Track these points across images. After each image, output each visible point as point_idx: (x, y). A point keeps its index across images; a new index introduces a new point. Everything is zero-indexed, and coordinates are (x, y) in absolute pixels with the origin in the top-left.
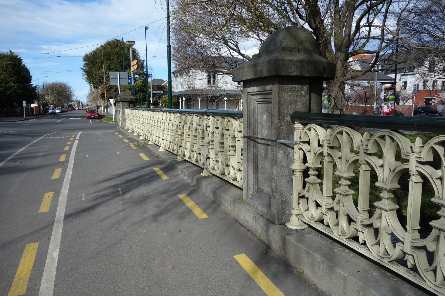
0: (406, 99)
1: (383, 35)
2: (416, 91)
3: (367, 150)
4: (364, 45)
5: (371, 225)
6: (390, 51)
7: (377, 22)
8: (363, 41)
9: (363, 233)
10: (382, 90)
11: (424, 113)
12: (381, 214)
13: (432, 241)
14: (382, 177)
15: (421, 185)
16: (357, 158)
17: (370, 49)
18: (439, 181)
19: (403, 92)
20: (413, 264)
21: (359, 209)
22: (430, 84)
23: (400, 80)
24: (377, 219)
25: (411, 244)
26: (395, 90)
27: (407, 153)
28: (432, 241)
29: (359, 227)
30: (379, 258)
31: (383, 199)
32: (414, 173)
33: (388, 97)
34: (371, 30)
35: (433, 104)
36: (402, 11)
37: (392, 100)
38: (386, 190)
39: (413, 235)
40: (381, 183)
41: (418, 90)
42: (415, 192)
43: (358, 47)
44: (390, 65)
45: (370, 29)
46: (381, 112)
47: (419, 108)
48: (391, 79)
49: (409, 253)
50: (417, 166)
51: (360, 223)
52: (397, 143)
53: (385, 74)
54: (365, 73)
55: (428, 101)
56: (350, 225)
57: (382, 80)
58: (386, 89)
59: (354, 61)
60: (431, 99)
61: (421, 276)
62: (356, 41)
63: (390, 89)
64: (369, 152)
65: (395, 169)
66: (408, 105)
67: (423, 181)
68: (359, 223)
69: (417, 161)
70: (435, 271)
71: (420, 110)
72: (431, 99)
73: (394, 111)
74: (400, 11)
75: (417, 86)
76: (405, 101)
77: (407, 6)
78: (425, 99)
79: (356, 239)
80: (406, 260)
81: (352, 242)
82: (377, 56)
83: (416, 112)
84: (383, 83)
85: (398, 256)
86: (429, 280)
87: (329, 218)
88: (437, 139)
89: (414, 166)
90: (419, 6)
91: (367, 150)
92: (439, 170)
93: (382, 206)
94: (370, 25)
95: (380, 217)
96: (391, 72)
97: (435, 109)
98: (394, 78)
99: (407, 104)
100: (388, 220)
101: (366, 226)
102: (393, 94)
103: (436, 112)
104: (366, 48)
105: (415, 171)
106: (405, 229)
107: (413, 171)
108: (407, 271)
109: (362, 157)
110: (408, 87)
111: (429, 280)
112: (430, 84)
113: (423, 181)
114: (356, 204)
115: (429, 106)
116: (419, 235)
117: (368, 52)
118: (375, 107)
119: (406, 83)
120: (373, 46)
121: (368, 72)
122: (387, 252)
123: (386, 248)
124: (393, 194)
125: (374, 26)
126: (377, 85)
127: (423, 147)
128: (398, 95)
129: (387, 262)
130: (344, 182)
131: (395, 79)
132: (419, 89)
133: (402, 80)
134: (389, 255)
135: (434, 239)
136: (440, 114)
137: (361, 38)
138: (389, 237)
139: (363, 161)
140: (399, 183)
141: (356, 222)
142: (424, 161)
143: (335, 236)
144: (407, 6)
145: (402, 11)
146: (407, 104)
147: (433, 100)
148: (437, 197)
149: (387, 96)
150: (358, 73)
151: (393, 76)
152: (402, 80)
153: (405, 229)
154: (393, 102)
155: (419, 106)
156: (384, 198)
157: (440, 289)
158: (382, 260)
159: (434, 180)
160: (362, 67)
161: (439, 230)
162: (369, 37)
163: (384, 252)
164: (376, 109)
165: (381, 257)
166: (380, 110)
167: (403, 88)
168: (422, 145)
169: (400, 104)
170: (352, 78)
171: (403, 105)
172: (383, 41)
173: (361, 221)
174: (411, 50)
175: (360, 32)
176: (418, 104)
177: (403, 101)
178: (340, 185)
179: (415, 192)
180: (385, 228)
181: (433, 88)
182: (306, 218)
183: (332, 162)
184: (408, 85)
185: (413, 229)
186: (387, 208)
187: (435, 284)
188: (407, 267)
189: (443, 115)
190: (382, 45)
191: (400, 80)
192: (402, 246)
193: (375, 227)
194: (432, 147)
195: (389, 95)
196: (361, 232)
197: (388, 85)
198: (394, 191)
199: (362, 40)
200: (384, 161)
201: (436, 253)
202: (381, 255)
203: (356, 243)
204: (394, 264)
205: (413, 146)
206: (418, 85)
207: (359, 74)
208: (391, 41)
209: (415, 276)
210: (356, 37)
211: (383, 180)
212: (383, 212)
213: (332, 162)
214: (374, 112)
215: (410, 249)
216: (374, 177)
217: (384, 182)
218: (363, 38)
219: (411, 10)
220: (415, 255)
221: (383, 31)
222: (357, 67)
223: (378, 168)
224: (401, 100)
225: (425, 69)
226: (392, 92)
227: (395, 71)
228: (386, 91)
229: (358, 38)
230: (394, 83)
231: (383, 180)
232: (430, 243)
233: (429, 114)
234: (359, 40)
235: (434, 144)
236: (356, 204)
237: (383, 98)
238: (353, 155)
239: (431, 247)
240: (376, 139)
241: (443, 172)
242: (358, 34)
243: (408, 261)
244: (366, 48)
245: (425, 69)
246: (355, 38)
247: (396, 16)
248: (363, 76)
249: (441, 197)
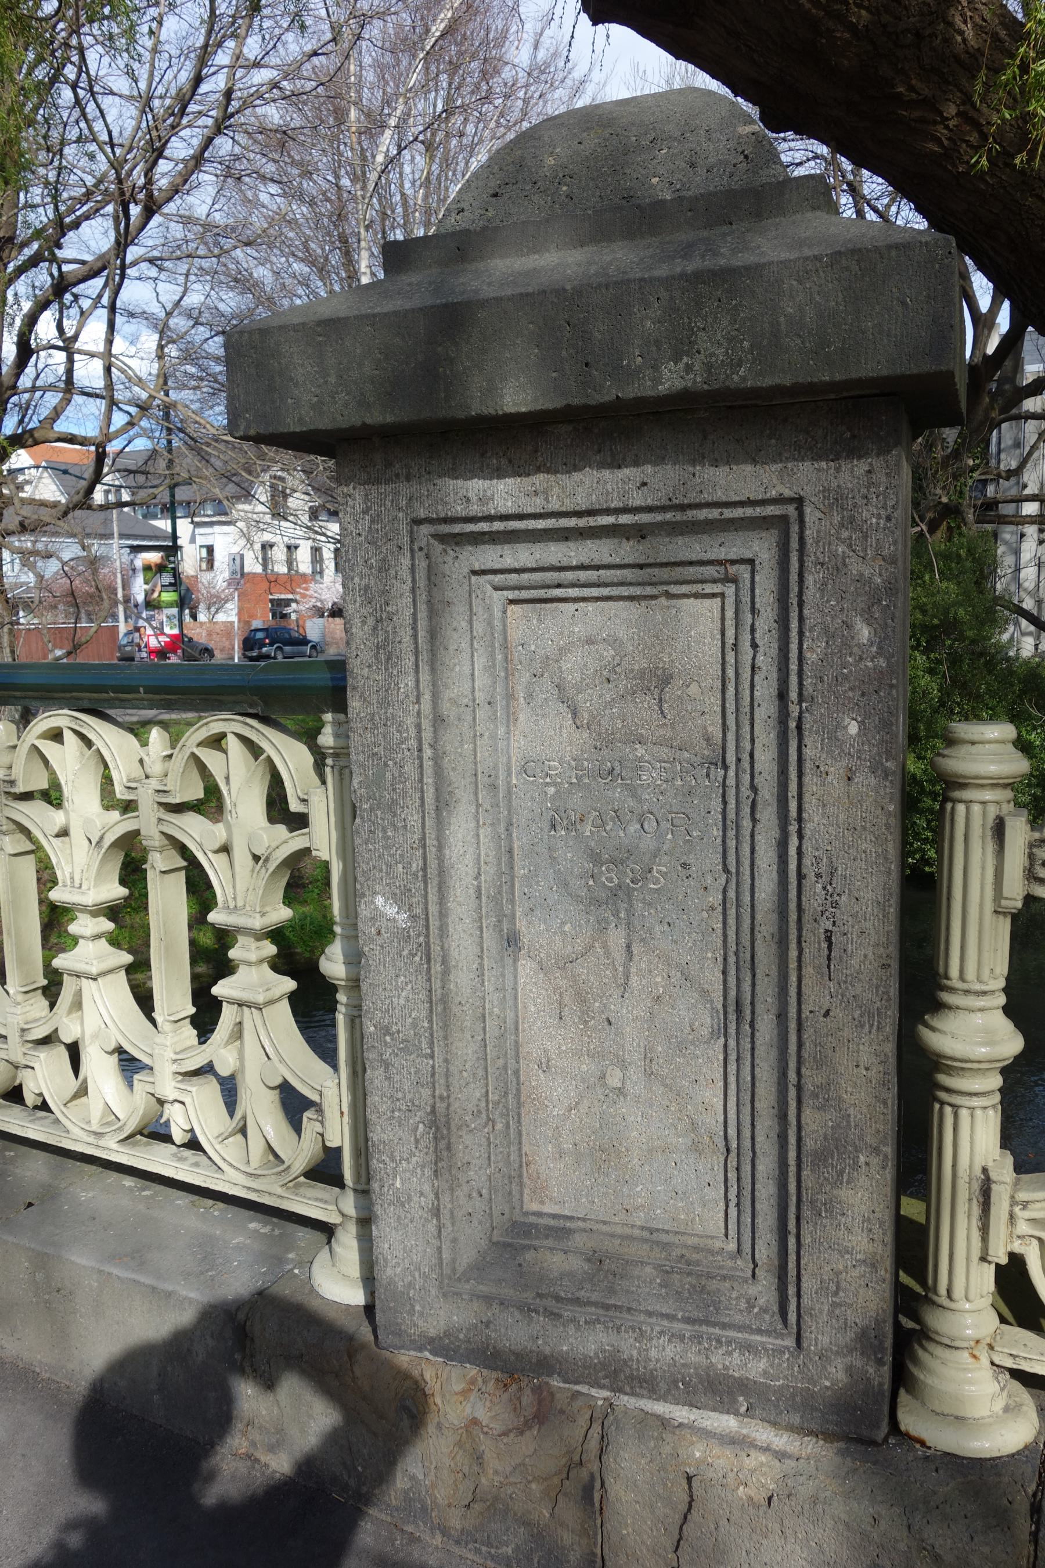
0: (217, 602)
1: (110, 386)
2: (239, 576)
3: (12, 783)
4: (57, 413)
5: (208, 1069)
6: (141, 444)
7: (93, 334)
8: (52, 399)
9: (183, 1103)
10: (134, 570)
11: (271, 644)
12: (79, 993)
13: (227, 1044)
14: (68, 870)
15: (182, 874)
16: (128, 825)
17: (74, 430)
18: (223, 856)
19: (205, 578)
20: (188, 1128)
21: (11, 992)
22: (279, 554)
23: (193, 540)
24: (70, 1012)
25: (175, 1068)
26: (175, 573)
27: (129, 781)
28: (227, 1044)
29: (168, 1088)
30: (91, 1139)
31: (81, 941)
32: (157, 844)
33: (156, 595)
34: (76, 365)
35: (293, 616)
36: (169, 314)
37: (170, 605)
38: (84, 909)
39: (176, 1039)
40: (69, 889)
41: (243, 574)
42: (168, 902)
43: (35, 418)
44: (152, 490)
45: (70, 361)
46: (139, 646)
47: (257, 630)
48: (157, 535)
49: (171, 1099)
50: (160, 820)
51: (18, 1039)
52: (98, 750)
53: (145, 516)
54: (65, 514)
55: (279, 608)
56: (131, 1085)
57: (136, 537)
58: (147, 568)
59: (37, 467)
60: (287, 603)
61: (210, 1158)
62: (26, 396)
63: (161, 568)
64: (20, 788)
65: (102, 838)
66: (223, 623)
67: (185, 864)
68: (14, 1038)
69: (160, 804)
70: (243, 1131)
71: (260, 635)
72: (287, 603)
73: (179, 642)
74: (163, 315)
75: (238, 562)
76: (213, 609)
77: (181, 299)
78: (272, 601)
79: (157, 1133)
80: (168, 1121)
81: (9, 1112)
82: (100, 457)
83: (249, 643)
84: (136, 549)
85: (144, 1116)
86: (231, 1165)
87: (196, 1111)
88: (204, 729)
89: (154, 820)
90: (222, 306)
91: (12, 783)
92: (220, 825)
93: (80, 967)
94: (68, 345)
95: (77, 1004)
96: (162, 512)
97: (301, 631)
98: (170, 530)
99: (221, 617)
100: (102, 1010)
101: (197, 1073)
102: (171, 584)
103: (304, 641)
104: (62, 426)
105: (157, 836)
106: (153, 1022)
107: (151, 838)
108: (174, 1155)
109: (148, 822)
110: (216, 564)
111: (231, 1165)
112: (279, 554)
113: (185, 864)
114: (144, 1000)
115: (283, 623)
116: (195, 1032)
117: (71, 439)
118: (123, 628)
119: (210, 550)
120: (83, 418)
121: (74, 508)
122: (276, 1156)
123: (269, 1138)
124: (110, 919)
125: (80, 352)
126: (116, 551)
127: (170, 756)
128: (188, 590)
129: (279, 1191)
130: (82, 926)
131: (174, 537)
132: (246, 570)
133: (200, 540)
134: (283, 1162)
135: (230, 1037)
136: (314, 647)
137: (45, 389)
138: (274, 1096)
139: (4, 821)
140: (123, 882)
141: (152, 1069)
142: (178, 801)
143: (79, 1142)
144: (181, 299)
145: (169, 314)
146: (221, 617)
147: (294, 605)
148: (223, 908)
149: (153, 591)
150: (44, 511)
151: (164, 524)
152: (200, 540)
153: (153, 1022)
154: (174, 611)
155: (257, 624)
156: (83, 937)
157: (261, 1180)
158: (101, 1143)
159: (210, 855)
160: (65, 488)
161: (240, 1005)
162: (69, 386)
163: (103, 1116)
164: (126, 635)
165: (96, 1134)
166: (137, 640)
167: (204, 566)
168: (169, 752)
169: (202, 617)
170: (23, 528)
171: (211, 621)
172: (113, 403)
173: (23, 1030)
174: (208, 445)
175: (40, 366)
176: (252, 616)
177: (209, 609)
178: (75, 940)
179: (168, 902)
180: (95, 1036)
181: (290, 569)
182: (75, 1131)
183: (32, 852)
184: (220, 556)
185: (172, 1018)
186: (94, 971)
187: (248, 1170)
188: (173, 1143)
189: (322, 652)
190: (109, 419)
191: (193, 540)
192: (151, 1079)
193: (224, 1071)
194: (193, 754)
195: (159, 588)
196: (27, 1067)
197: (154, 557)
198: (112, 912)
199: (48, 394)
200: (67, 813)
201: (239, 1077)
202: (95, 1127)
203: (17, 1108)
204: (135, 1144)
205: (146, 759)
206: (242, 557)
207: (45, 515)
208: (143, 408)
209: (196, 1165)
210: (25, 381)
211: (72, 878)
212: (85, 983)
213: (32, 852)
214: (120, 648)
215: (174, 1084)
216: (199, 889)
217: (77, 883)
218: (51, 387)
219: (195, 314)
220: (187, 1100)
221: (108, 370)
222: (48, 489)
223: (53, 840)
224: (202, 607)
225: (259, 507)
226: (167, 578)
227: (170, 510)
228: (150, 574)
229: (34, 389)
230: (172, 549)
231: (72, 878)
232: (223, 1051)
233: (287, 649)
234: (38, 394)
235: (199, 745)
236: (144, 1000)
237: (140, 598)
238: (115, 815)
239: (226, 1062)
240: (37, 743)
241: (229, 828)
242: (30, 371)
243: (172, 1124)
244: (62, 426)
245: (259, 507)
246: (20, 383)
247: (155, 326)
248: (61, 523)
249: (232, 905)
